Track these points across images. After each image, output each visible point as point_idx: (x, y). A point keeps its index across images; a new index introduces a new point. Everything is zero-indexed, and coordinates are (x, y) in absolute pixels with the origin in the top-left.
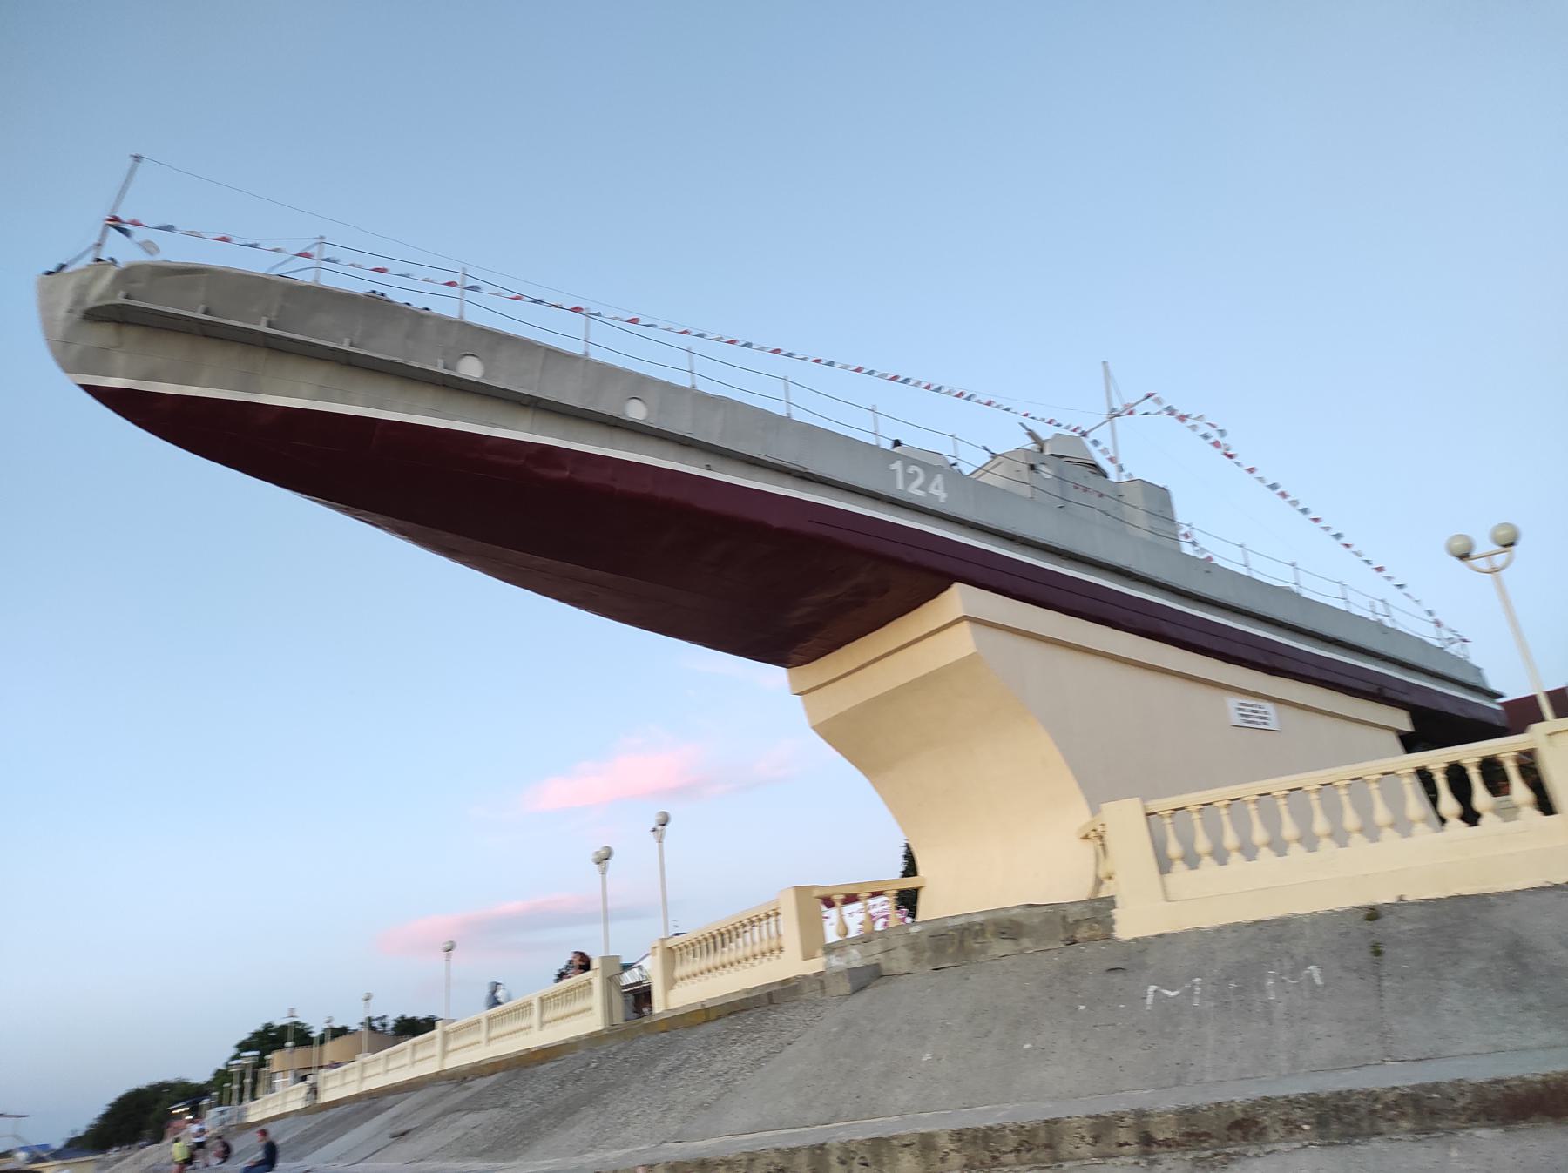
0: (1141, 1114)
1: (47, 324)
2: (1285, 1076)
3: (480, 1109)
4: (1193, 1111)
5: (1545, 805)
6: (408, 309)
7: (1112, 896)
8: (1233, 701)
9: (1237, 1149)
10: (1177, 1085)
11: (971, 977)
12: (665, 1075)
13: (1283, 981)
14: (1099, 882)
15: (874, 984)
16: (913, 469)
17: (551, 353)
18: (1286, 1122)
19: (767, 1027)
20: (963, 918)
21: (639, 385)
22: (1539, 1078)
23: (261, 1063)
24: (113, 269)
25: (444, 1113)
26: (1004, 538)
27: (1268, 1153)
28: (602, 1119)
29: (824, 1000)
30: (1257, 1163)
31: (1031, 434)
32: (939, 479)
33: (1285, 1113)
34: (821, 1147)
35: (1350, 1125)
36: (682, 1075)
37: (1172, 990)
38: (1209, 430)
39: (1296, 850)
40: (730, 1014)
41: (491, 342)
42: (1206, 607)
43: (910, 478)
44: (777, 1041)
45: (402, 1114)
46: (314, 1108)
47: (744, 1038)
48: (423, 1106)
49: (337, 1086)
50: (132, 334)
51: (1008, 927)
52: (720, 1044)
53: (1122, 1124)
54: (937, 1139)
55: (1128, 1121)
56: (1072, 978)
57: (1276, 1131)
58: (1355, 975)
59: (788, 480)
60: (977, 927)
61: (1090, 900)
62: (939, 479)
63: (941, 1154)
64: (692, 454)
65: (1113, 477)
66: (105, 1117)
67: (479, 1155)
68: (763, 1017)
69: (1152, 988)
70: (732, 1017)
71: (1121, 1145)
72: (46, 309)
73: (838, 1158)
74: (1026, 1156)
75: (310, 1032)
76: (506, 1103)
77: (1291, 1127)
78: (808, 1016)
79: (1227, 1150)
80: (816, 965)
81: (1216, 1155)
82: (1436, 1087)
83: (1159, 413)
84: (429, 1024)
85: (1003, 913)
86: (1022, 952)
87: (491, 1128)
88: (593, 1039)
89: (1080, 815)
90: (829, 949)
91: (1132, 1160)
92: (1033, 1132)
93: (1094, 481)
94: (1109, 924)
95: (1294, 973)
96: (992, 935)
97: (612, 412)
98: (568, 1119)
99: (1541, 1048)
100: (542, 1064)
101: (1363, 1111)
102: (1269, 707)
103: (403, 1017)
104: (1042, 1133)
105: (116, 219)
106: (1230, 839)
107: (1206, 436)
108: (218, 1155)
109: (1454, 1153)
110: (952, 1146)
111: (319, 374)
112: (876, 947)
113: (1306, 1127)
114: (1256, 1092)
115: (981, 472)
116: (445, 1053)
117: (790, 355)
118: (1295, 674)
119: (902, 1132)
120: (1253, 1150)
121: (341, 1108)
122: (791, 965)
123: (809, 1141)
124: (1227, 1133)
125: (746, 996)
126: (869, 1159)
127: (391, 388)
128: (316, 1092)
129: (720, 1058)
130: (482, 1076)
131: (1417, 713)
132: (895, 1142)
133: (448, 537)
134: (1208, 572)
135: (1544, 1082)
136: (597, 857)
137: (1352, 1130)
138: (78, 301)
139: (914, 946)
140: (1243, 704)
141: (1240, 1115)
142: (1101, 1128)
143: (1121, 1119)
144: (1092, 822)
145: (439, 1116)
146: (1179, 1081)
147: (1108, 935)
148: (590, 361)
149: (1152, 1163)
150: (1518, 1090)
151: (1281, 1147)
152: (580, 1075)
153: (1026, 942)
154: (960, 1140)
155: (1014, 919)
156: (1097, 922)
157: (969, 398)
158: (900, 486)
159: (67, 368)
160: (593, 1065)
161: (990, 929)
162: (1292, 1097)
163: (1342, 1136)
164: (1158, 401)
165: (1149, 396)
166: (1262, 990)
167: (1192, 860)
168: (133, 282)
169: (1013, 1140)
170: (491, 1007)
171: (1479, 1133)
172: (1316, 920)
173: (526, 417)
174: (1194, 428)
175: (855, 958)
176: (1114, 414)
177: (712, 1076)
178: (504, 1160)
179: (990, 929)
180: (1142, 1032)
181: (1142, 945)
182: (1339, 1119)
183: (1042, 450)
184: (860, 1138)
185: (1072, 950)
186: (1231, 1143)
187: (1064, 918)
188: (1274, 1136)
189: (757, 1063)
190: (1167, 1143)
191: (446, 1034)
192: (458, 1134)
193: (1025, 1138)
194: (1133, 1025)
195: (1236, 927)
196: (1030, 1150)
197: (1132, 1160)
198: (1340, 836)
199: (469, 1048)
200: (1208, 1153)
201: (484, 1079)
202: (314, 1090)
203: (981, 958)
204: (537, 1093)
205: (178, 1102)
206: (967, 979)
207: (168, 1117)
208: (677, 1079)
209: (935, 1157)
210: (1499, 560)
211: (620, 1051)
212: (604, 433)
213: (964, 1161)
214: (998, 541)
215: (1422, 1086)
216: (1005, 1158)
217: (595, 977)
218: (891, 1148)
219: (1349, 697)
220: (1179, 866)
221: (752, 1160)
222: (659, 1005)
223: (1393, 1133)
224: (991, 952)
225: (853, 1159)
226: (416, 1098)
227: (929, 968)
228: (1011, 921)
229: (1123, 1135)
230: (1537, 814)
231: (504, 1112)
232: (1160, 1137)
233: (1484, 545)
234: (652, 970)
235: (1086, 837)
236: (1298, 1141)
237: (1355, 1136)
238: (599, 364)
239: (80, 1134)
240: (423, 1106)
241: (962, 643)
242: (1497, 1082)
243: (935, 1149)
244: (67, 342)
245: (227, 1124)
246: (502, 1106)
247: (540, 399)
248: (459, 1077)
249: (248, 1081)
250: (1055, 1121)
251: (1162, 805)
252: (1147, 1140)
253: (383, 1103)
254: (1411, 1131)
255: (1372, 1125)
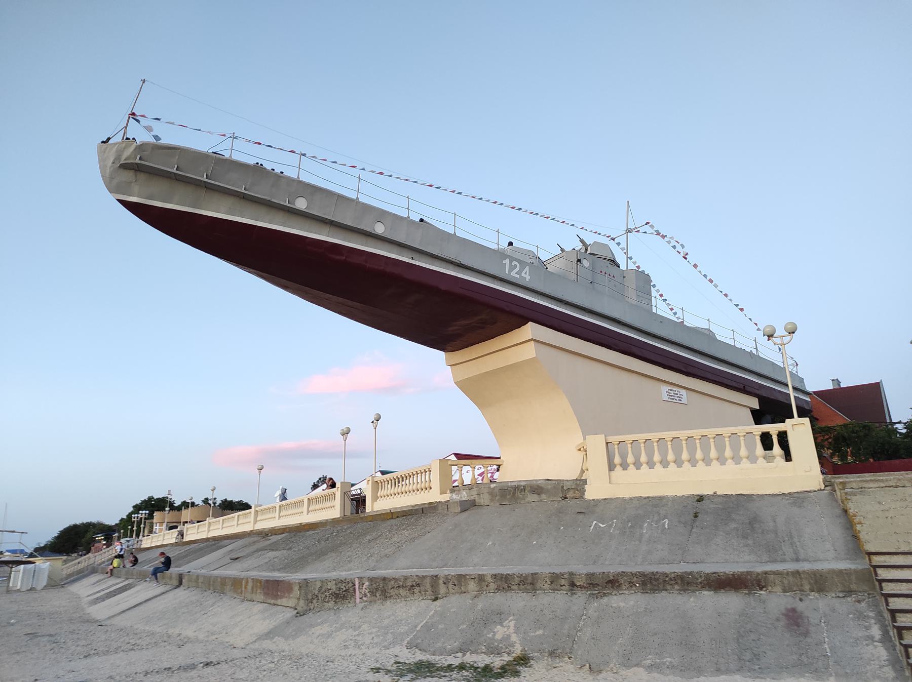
0: (571, 574)
1: (102, 169)
2: (638, 565)
3: (277, 550)
4: (593, 574)
5: (788, 457)
6: (272, 173)
7: (586, 479)
8: (665, 388)
9: (608, 591)
10: (593, 564)
11: (516, 510)
12: (370, 541)
13: (652, 525)
14: (583, 471)
15: (472, 509)
16: (514, 263)
17: (340, 197)
18: (630, 582)
19: (420, 524)
20: (516, 482)
21: (382, 215)
22: (731, 573)
23: (151, 516)
24: (134, 145)
25: (258, 551)
26: (557, 300)
27: (620, 594)
28: (339, 558)
29: (447, 514)
30: (615, 597)
31: (582, 241)
32: (527, 269)
33: (630, 579)
34: (436, 576)
35: (655, 585)
36: (378, 542)
37: (603, 524)
38: (676, 244)
39: (672, 466)
40: (403, 516)
41: (312, 191)
42: (657, 340)
43: (512, 268)
44: (423, 531)
45: (233, 549)
46: (181, 543)
47: (408, 528)
48: (245, 546)
49: (193, 533)
50: (142, 176)
51: (536, 488)
52: (396, 530)
53: (563, 577)
54: (486, 577)
55: (566, 576)
56: (560, 515)
57: (625, 586)
58: (682, 525)
59: (451, 266)
60: (522, 487)
61: (576, 480)
62: (527, 269)
63: (487, 583)
64: (405, 251)
65: (623, 267)
66: (56, 538)
67: (279, 570)
68: (418, 519)
69: (595, 522)
70: (405, 517)
71: (561, 586)
72: (102, 160)
73: (443, 581)
74: (522, 587)
75: (175, 503)
76: (290, 548)
77: (632, 584)
78: (439, 520)
79: (605, 592)
80: (446, 497)
81: (599, 593)
82: (691, 573)
83: (652, 234)
84: (245, 506)
85: (535, 482)
86: (541, 501)
87: (283, 559)
88: (334, 522)
89: (578, 439)
90: (454, 489)
91: (565, 592)
92: (526, 577)
93: (612, 269)
94: (583, 492)
95: (657, 522)
96: (528, 491)
97: (368, 229)
98: (322, 557)
99: (744, 562)
100: (308, 531)
101: (661, 581)
102: (683, 392)
103: (226, 500)
104: (530, 578)
105: (133, 114)
106: (643, 458)
107: (674, 247)
108: (131, 562)
109: (692, 599)
110: (492, 581)
111: (229, 201)
112: (474, 492)
113: (638, 585)
114: (621, 569)
115: (557, 257)
116: (256, 521)
117: (460, 193)
118: (700, 376)
119: (471, 573)
120: (614, 592)
121: (196, 544)
122: (435, 496)
123: (432, 574)
124: (606, 584)
125: (412, 508)
126: (456, 583)
127: (263, 211)
128: (182, 536)
129: (396, 536)
130: (276, 535)
131: (762, 400)
132: (468, 577)
133: (284, 281)
134: (661, 322)
135: (733, 575)
136: (342, 432)
137: (656, 588)
138: (118, 158)
139: (492, 493)
140: (669, 390)
141: (612, 578)
142: (554, 578)
143: (563, 575)
144: (583, 443)
145: (254, 552)
146: (594, 563)
147: (582, 497)
148: (359, 202)
149: (572, 594)
150: (722, 577)
151: (627, 592)
152: (328, 538)
153: (544, 496)
154: (495, 578)
155: (540, 485)
156: (577, 490)
157: (552, 219)
158: (507, 272)
159: (111, 191)
160: (334, 534)
161: (528, 489)
162: (633, 573)
163: (651, 590)
164: (652, 227)
165: (647, 223)
166: (641, 527)
167: (625, 466)
168: (144, 151)
169: (517, 580)
170: (282, 501)
171: (703, 592)
172: (676, 499)
173: (326, 229)
174: (669, 242)
175: (464, 496)
176: (629, 231)
177: (391, 544)
178: (291, 573)
179: (528, 489)
180: (585, 541)
181: (596, 502)
182: (651, 583)
183: (586, 250)
184: (453, 574)
185: (564, 502)
186: (606, 589)
187: (563, 487)
188: (624, 588)
189: (413, 539)
190: (581, 587)
191: (257, 512)
192: (267, 560)
193: (522, 579)
194: (582, 538)
195: (639, 499)
196: (523, 585)
197: (565, 592)
198: (693, 462)
199: (270, 520)
200: (596, 592)
201: (277, 536)
202: (181, 534)
203: (523, 502)
204: (306, 545)
205: (99, 534)
206: (514, 510)
207: (93, 541)
208: (375, 543)
209: (484, 584)
210: (786, 339)
211: (348, 528)
212: (363, 239)
213: (496, 587)
214: (553, 302)
215: (685, 573)
216: (513, 587)
217: (337, 491)
218: (466, 579)
219: (727, 390)
220: (618, 468)
221: (406, 579)
222: (369, 507)
223: (671, 590)
224: (527, 500)
225: (449, 582)
226: (240, 543)
227: (498, 504)
228: (538, 486)
229: (563, 582)
230: (783, 461)
231: (289, 552)
232: (578, 584)
233: (780, 331)
234: (365, 488)
235: (580, 450)
236: (634, 590)
237: (656, 590)
238: (363, 204)
239: (42, 545)
240: (245, 546)
241: (529, 352)
242: (715, 573)
243: (484, 581)
244: (112, 178)
245: (131, 547)
246: (288, 549)
247: (333, 221)
248: (264, 534)
249: (142, 526)
250: (536, 574)
251: (614, 439)
252: (573, 585)
253: (222, 543)
254: (679, 590)
255: (664, 586)
